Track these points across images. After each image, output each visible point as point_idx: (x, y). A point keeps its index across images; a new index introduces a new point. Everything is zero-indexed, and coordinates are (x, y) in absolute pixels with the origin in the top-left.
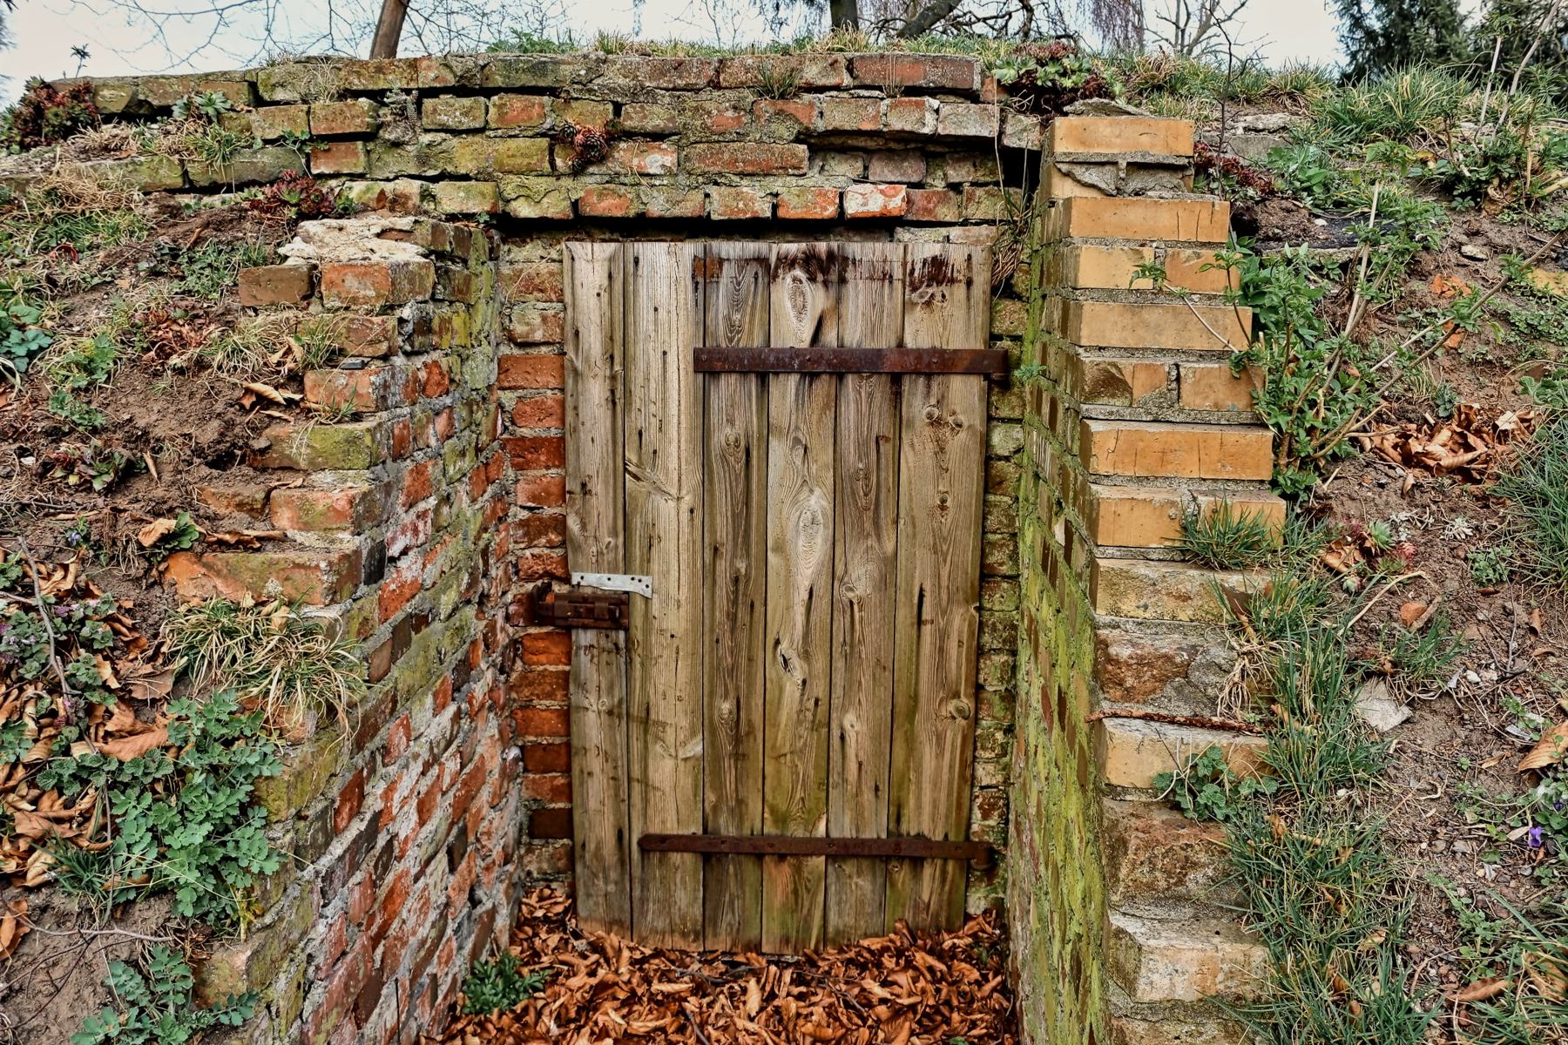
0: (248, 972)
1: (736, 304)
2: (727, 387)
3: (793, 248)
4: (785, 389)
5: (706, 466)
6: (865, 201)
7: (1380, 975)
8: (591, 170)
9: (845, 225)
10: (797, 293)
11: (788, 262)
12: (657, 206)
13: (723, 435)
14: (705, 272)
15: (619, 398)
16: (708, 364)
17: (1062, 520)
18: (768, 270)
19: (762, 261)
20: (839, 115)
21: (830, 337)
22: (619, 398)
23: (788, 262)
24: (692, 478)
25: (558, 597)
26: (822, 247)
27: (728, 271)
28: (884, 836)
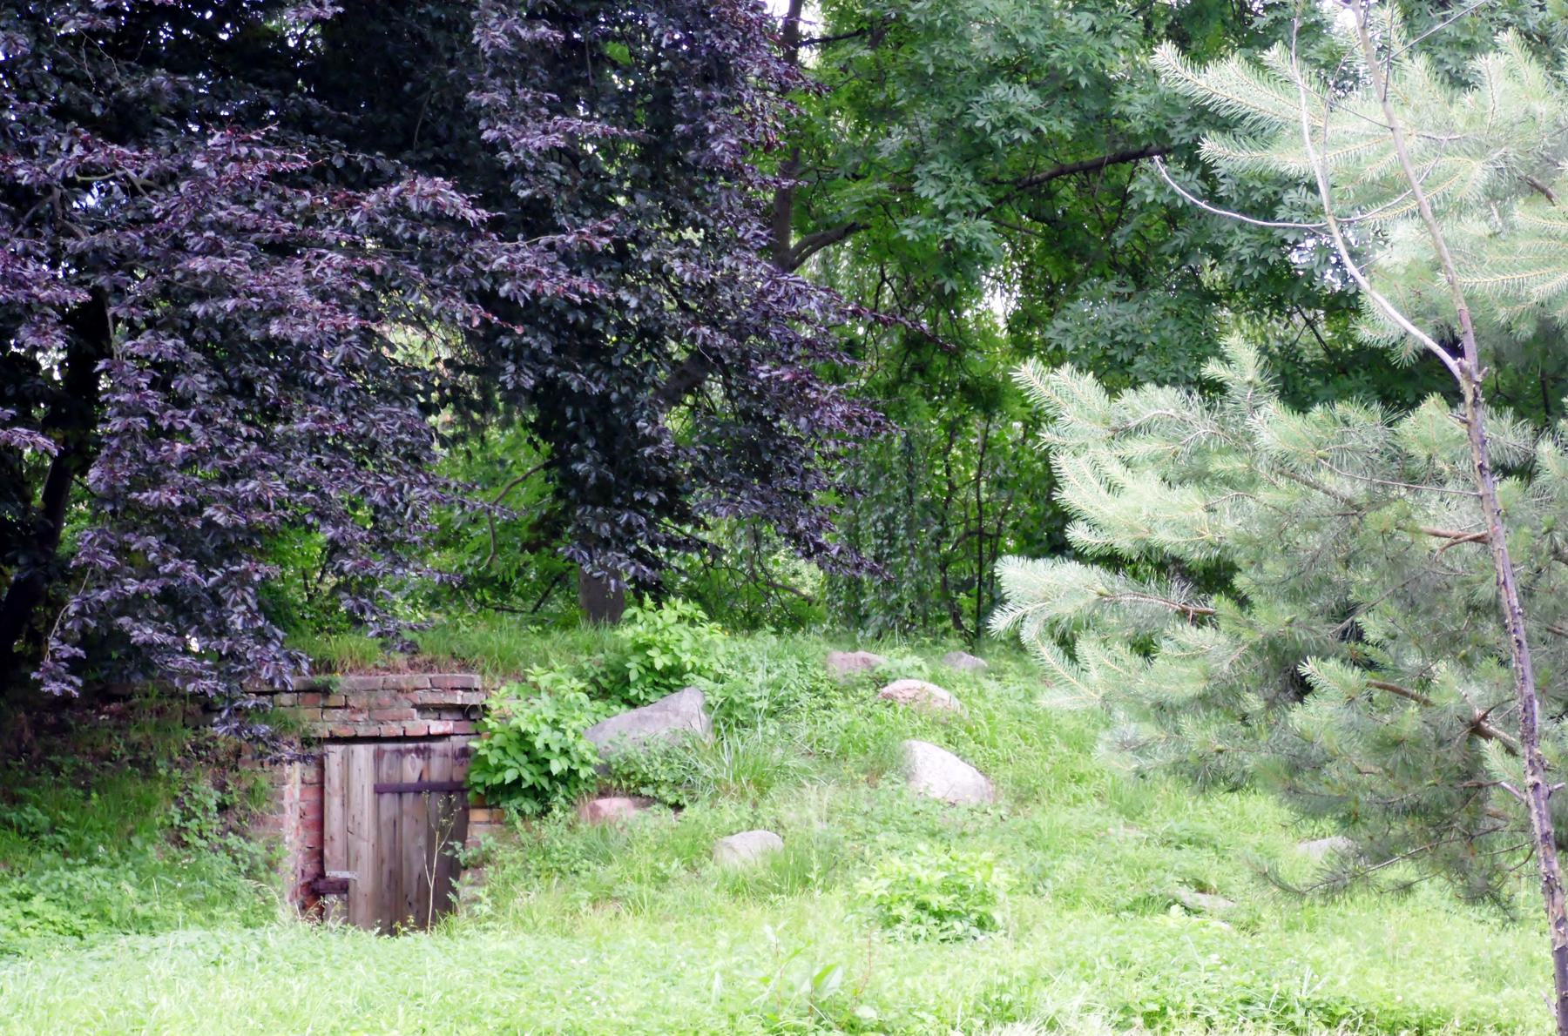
0: (416, 369)
1: (390, 767)
2: (387, 798)
3: (410, 746)
4: (409, 798)
5: (379, 829)
6: (437, 727)
7: (289, 193)
8: (108, 566)
9: (430, 737)
10: (413, 762)
11: (409, 751)
12: (362, 732)
13: (384, 816)
14: (378, 756)
15: (346, 803)
16: (379, 790)
17: (180, 563)
18: (401, 754)
19: (399, 751)
20: (430, 698)
21: (425, 778)
22: (346, 803)
23: (409, 751)
24: (373, 833)
25: (209, 523)
26: (422, 745)
27: (386, 756)
28: (1091, 374)
